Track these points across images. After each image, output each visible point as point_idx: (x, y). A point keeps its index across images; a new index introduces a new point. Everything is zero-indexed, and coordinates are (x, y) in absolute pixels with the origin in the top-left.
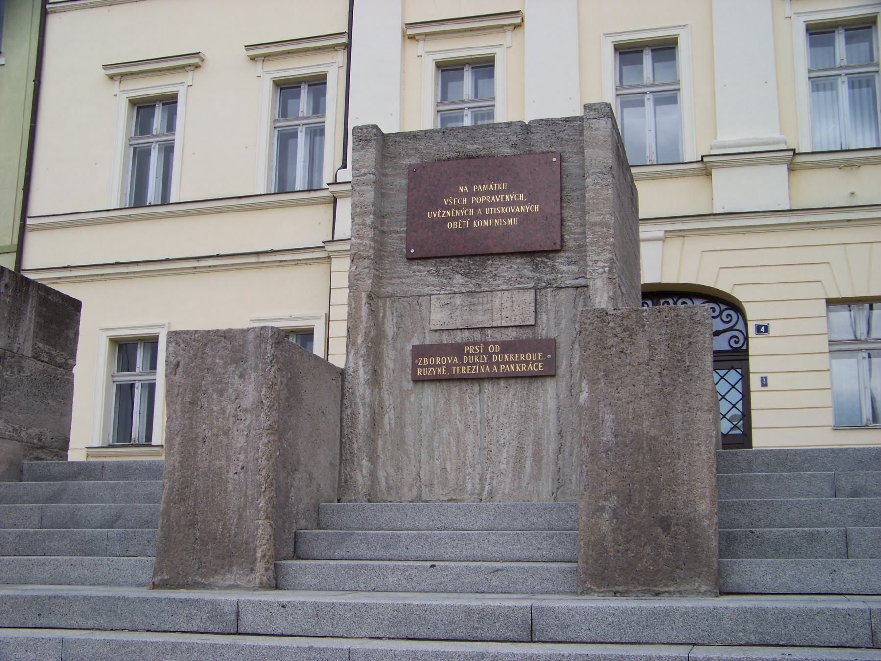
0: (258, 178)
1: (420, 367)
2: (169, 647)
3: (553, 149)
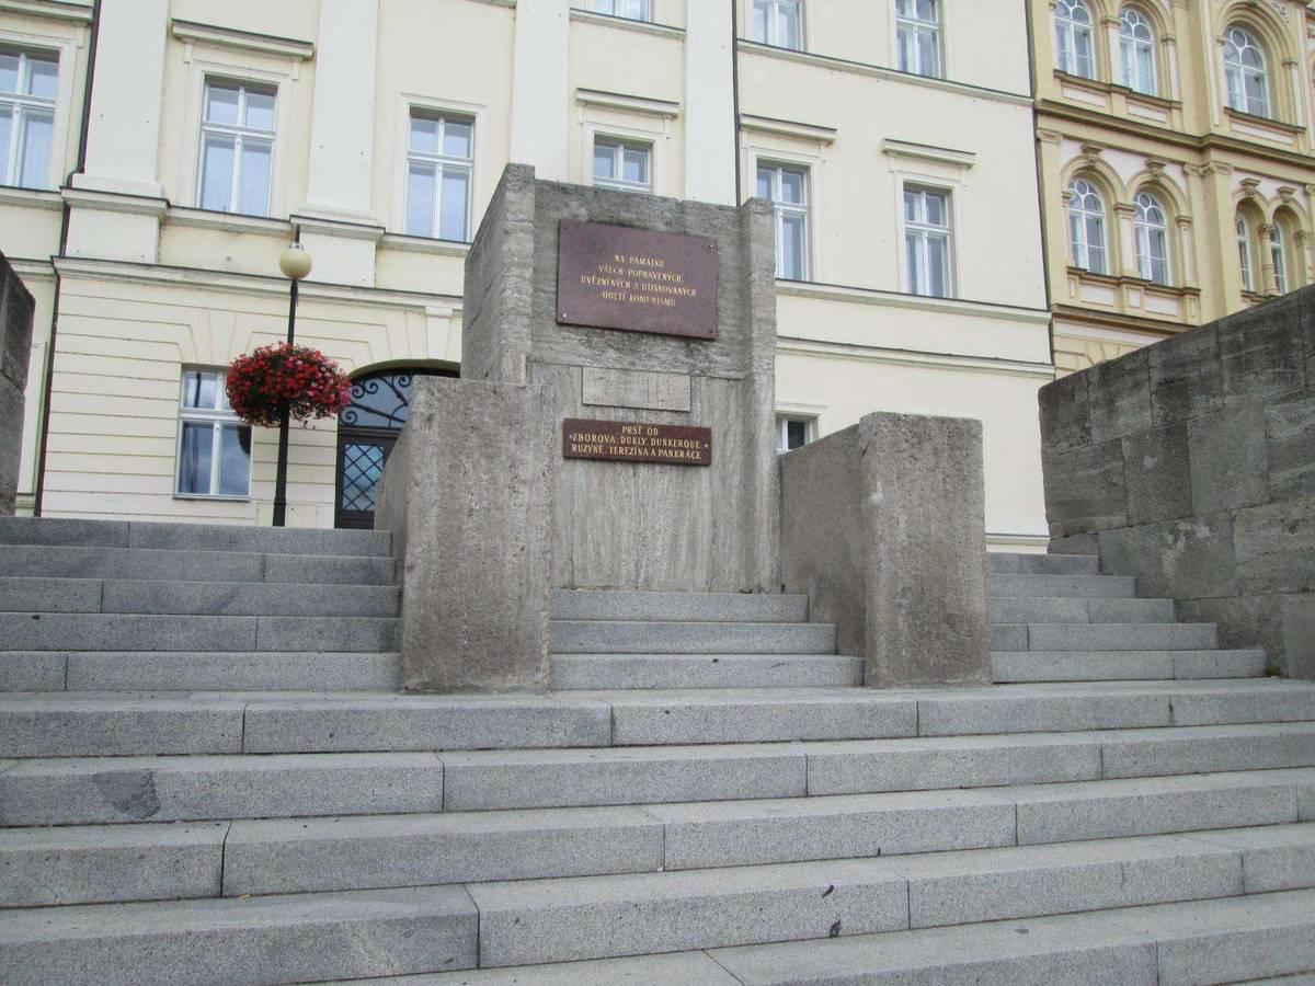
3: (706, 235)
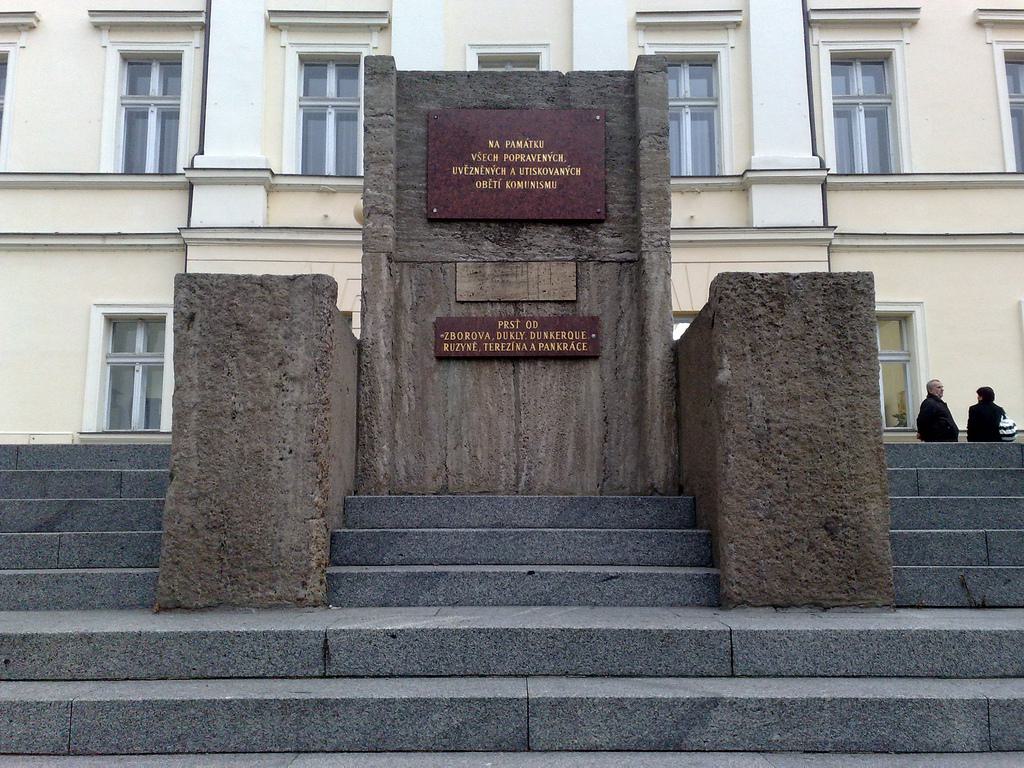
0: (109, 158)
1: (446, 342)
2: (251, 707)
